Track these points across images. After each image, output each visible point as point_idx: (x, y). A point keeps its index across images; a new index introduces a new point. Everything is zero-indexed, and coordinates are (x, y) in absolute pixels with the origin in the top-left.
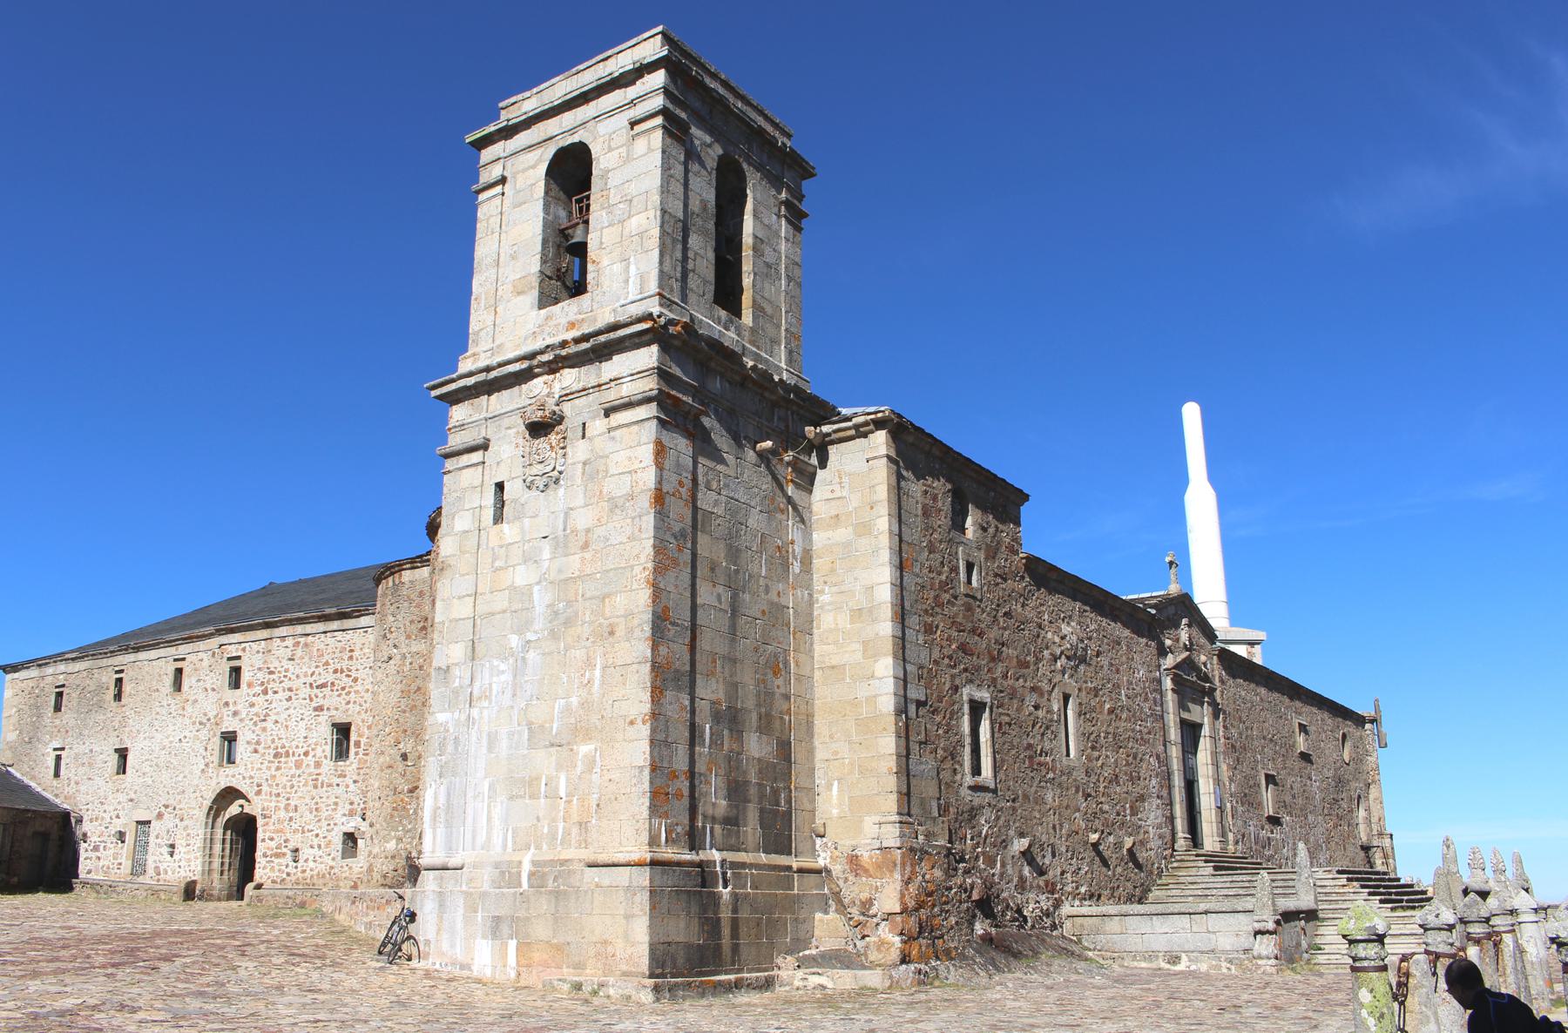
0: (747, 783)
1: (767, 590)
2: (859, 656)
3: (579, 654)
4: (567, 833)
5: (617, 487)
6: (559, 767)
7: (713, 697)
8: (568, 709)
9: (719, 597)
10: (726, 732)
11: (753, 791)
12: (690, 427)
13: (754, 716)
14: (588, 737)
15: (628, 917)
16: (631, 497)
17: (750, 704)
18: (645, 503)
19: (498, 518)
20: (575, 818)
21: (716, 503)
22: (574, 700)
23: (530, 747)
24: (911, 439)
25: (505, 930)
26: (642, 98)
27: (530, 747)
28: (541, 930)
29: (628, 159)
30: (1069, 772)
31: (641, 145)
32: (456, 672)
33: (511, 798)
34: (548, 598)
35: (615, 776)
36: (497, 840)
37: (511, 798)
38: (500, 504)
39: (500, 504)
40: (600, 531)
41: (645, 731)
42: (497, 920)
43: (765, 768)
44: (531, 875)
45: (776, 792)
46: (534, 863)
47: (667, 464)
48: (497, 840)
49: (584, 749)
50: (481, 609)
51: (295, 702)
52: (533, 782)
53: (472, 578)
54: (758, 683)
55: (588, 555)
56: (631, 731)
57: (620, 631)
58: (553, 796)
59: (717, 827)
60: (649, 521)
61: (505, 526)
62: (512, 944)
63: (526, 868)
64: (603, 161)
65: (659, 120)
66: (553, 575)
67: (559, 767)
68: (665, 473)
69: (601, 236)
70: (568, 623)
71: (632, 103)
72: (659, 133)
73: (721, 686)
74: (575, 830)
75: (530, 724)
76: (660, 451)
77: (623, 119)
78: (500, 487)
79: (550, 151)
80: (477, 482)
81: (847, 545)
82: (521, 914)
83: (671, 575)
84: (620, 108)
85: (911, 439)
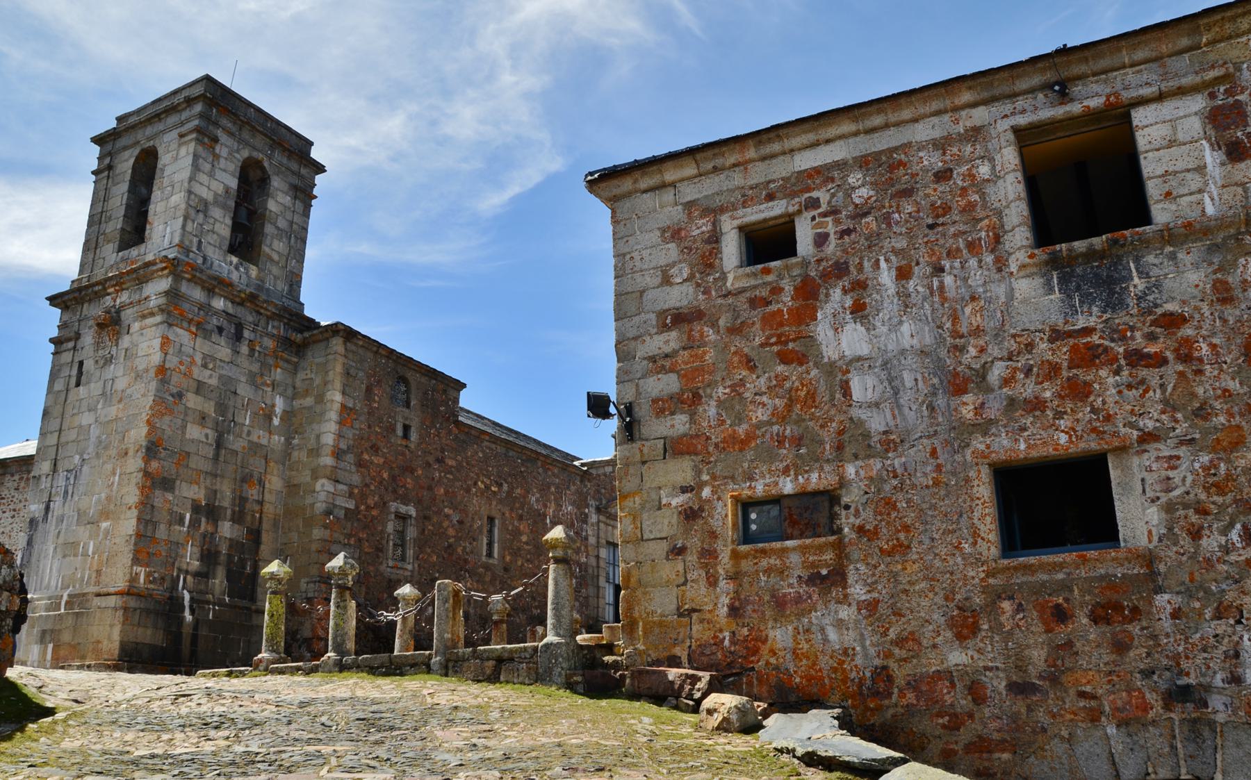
0: (218, 553)
1: (249, 433)
2: (308, 479)
3: (109, 467)
4: (90, 578)
5: (141, 364)
6: (90, 537)
7: (195, 497)
8: (99, 500)
9: (207, 436)
10: (203, 520)
11: (223, 558)
12: (194, 329)
13: (229, 512)
14: (107, 518)
15: (111, 626)
16: (147, 370)
17: (226, 503)
18: (152, 373)
19: (78, 385)
20: (95, 567)
21: (211, 377)
22: (103, 495)
23: (78, 525)
24: (361, 343)
25: (48, 638)
26: (188, 120)
27: (78, 525)
28: (66, 637)
29: (176, 159)
30: (487, 567)
31: (183, 151)
32: (43, 479)
33: (64, 556)
34: (97, 432)
35: (117, 541)
36: (53, 583)
37: (64, 556)
38: (80, 373)
39: (80, 373)
40: (128, 391)
41: (135, 512)
42: (44, 632)
43: (233, 544)
44: (67, 603)
45: (242, 562)
46: (69, 596)
47: (171, 351)
48: (53, 583)
49: (104, 525)
50: (63, 440)
51: (17, 520)
52: (75, 545)
53: (59, 420)
54: (234, 491)
55: (121, 406)
56: (129, 512)
57: (131, 453)
58: (85, 555)
59: (189, 578)
60: (153, 385)
61: (81, 388)
62: (51, 646)
63: (65, 598)
64: (164, 159)
65: (194, 135)
66: (102, 419)
67: (90, 537)
68: (168, 357)
69: (157, 208)
70: (106, 448)
71: (182, 124)
72: (193, 144)
73: (203, 492)
74: (94, 575)
75: (79, 510)
76: (166, 342)
77: (174, 134)
78: (81, 363)
79: (136, 151)
80: (69, 360)
81: (310, 408)
82: (58, 627)
83: (167, 419)
84: (175, 126)
85: (361, 343)
